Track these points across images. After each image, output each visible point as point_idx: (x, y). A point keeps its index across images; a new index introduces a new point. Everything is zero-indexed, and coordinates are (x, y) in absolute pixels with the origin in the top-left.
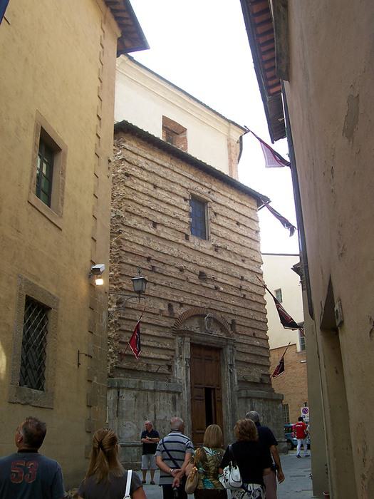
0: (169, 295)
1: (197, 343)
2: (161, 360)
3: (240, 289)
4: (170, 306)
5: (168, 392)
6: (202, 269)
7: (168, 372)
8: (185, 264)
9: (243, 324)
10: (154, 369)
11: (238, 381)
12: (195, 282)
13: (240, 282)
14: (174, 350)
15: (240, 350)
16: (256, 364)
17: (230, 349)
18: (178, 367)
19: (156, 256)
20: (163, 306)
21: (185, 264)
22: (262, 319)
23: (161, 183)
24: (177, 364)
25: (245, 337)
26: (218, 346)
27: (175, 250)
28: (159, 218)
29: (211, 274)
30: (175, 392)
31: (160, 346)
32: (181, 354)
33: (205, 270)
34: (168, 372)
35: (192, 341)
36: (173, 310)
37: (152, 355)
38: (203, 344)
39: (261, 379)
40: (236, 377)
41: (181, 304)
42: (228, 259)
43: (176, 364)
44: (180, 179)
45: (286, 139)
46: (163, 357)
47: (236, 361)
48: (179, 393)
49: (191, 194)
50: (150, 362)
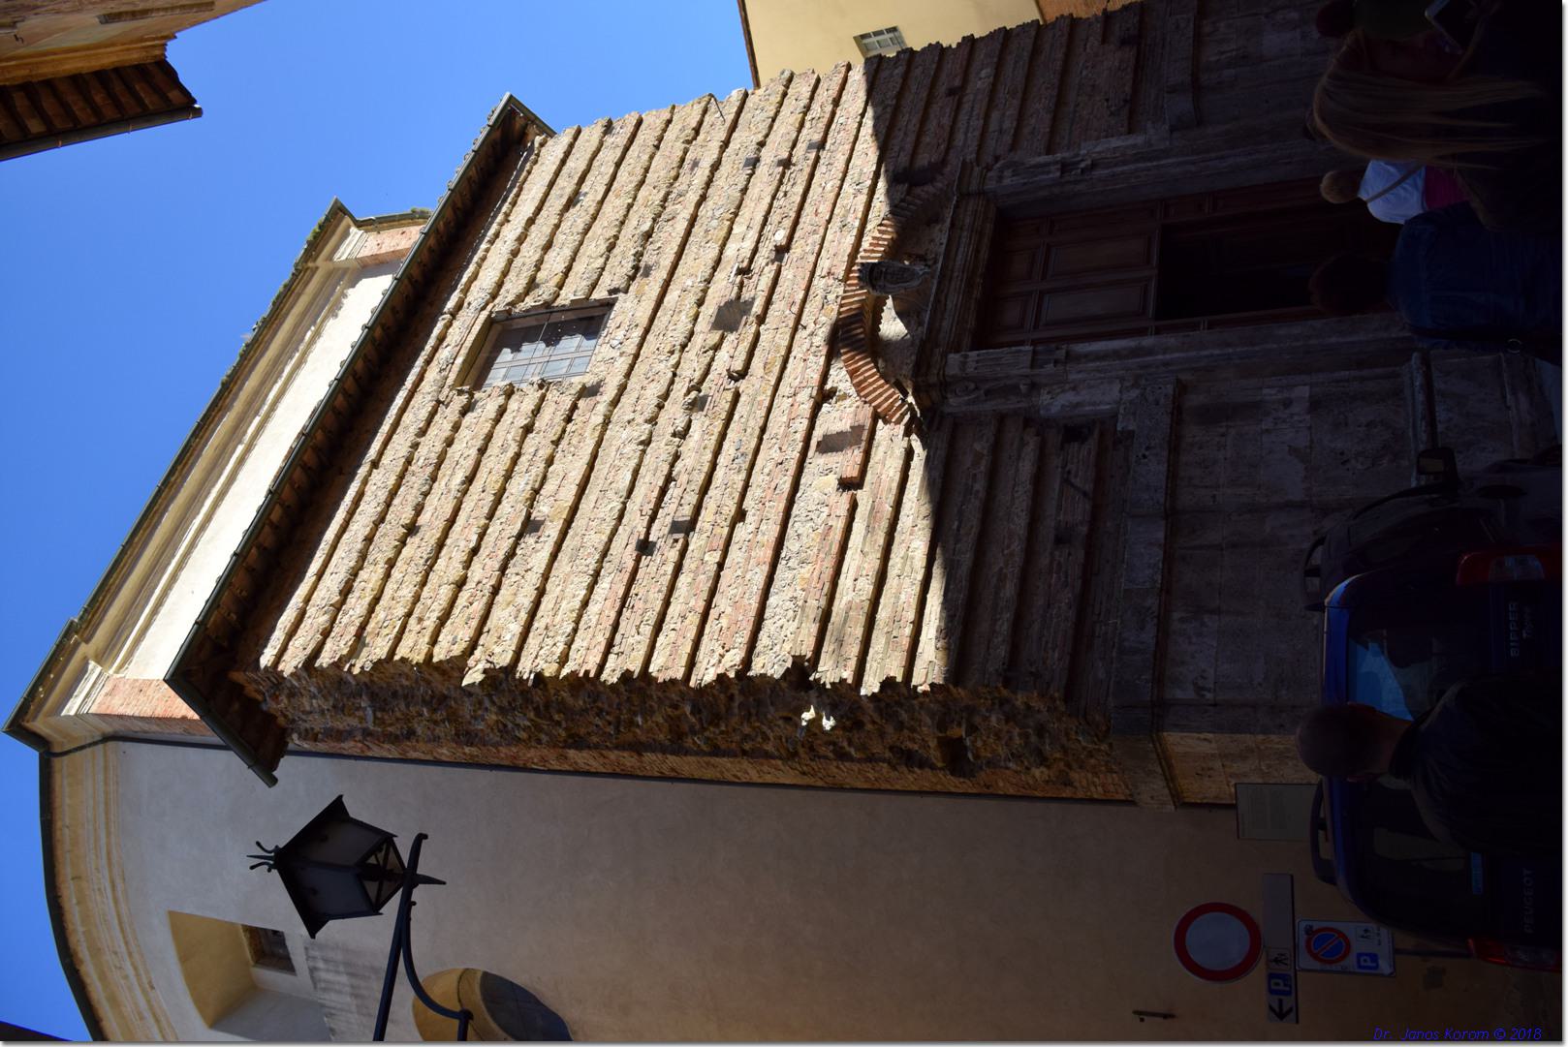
0: (778, 453)
1: (971, 323)
2: (1039, 479)
3: (786, 164)
4: (830, 445)
5: (1174, 445)
6: (703, 324)
7: (1092, 443)
8: (680, 388)
9: (911, 138)
10: (1078, 512)
11: (1130, 131)
12: (745, 345)
13: (762, 170)
14: (1002, 418)
15: (1008, 139)
16: (1065, 72)
17: (1000, 178)
18: (1069, 397)
19: (634, 523)
20: (823, 475)
21: (680, 388)
22: (900, 70)
23: (401, 512)
24: (1054, 403)
25: (961, 125)
26: (989, 227)
27: (623, 439)
28: (511, 513)
29: (722, 289)
30: (1177, 412)
31: (979, 486)
32: (1014, 389)
33: (709, 310)
34: (1092, 443)
35: (967, 340)
36: (841, 434)
37: (1020, 523)
38: (977, 293)
39: (1124, 42)
40: (1115, 142)
41: (824, 396)
42: (681, 226)
43: (1055, 409)
44: (891, 639)
45: (377, 883)
46: (1026, 468)
47: (1049, 151)
48: (1182, 388)
49: (754, 299)
50: (1047, 529)
